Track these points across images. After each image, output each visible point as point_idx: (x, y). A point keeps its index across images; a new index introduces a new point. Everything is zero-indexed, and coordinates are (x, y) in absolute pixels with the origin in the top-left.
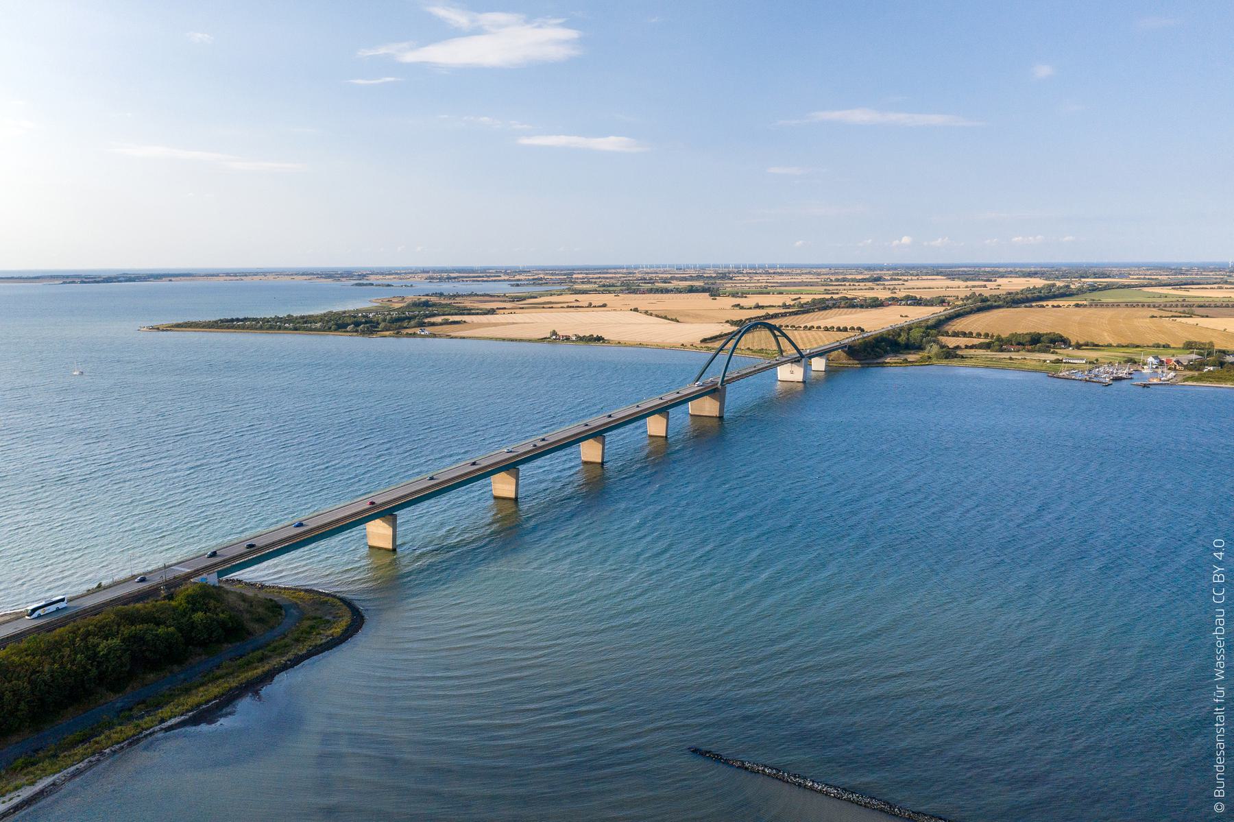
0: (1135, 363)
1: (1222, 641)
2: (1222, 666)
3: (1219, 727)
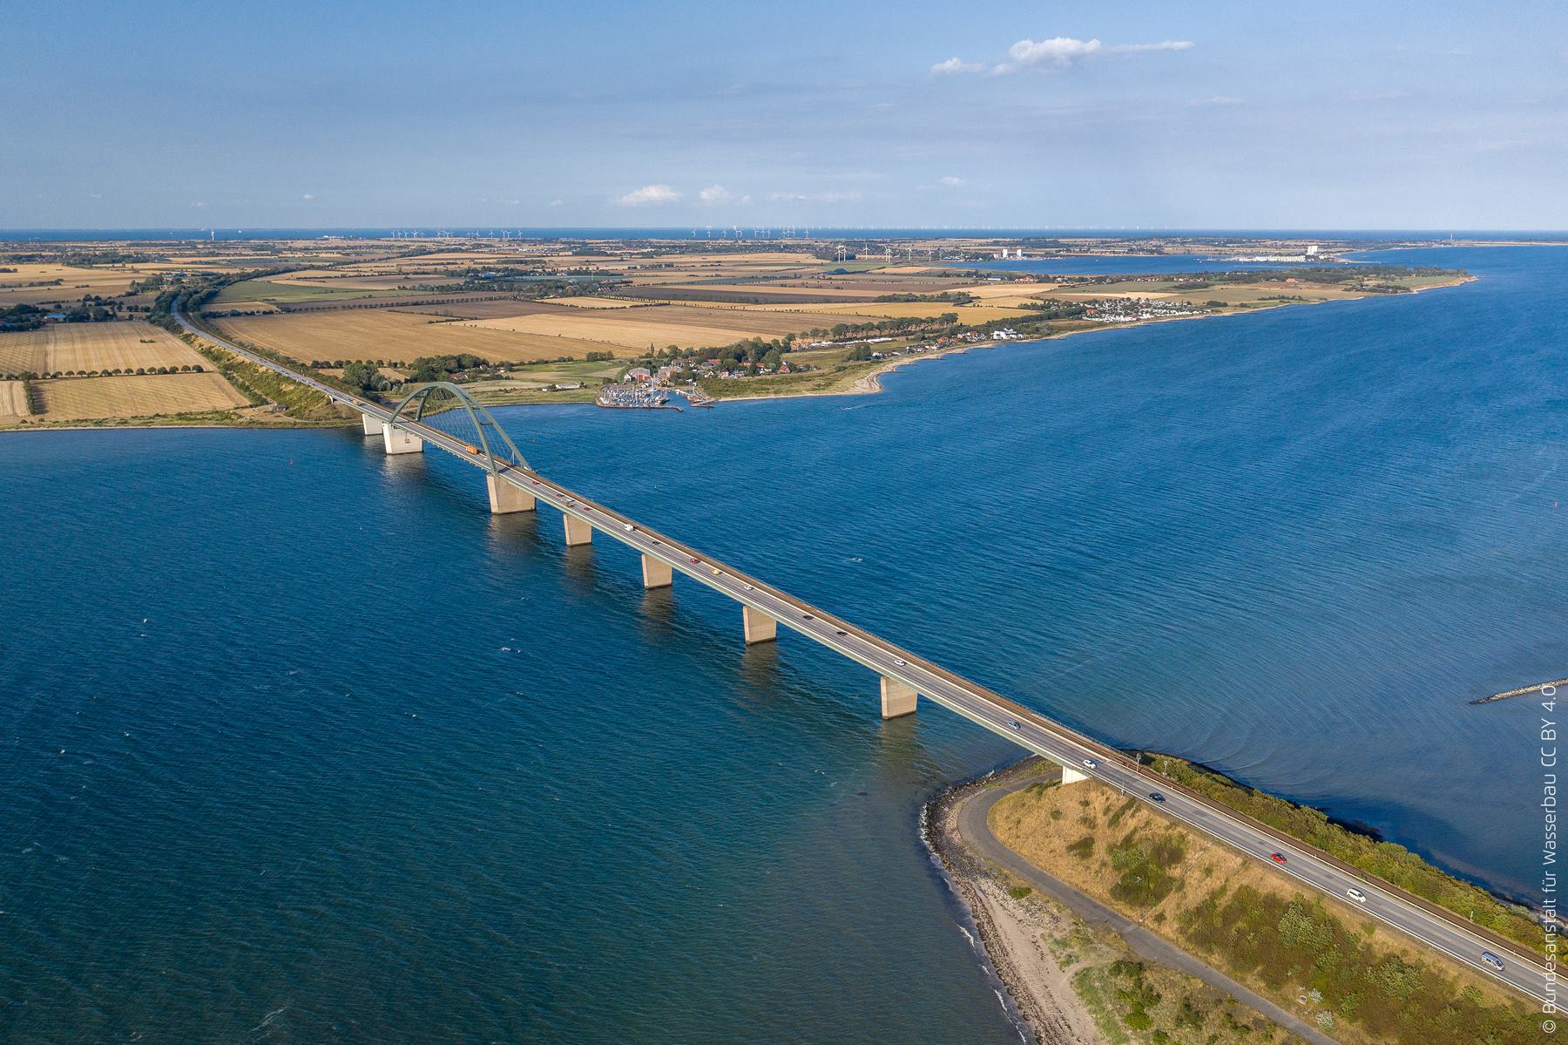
1: (1553, 814)
2: (1553, 846)
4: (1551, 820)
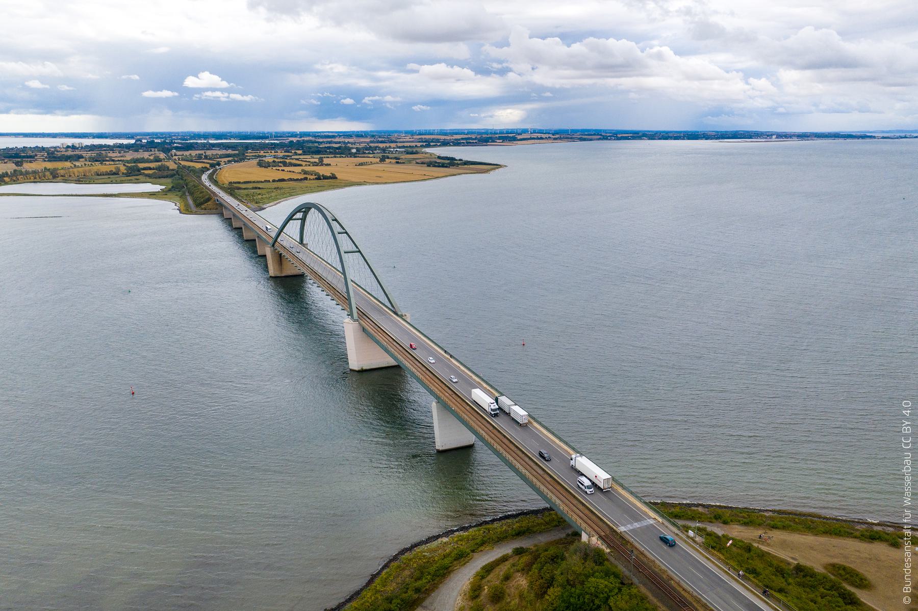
3: (907, 541)
4: (908, 480)
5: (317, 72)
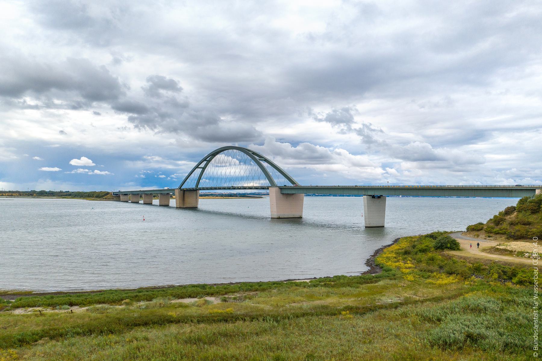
0: (480, 311)
5: (144, 160)
